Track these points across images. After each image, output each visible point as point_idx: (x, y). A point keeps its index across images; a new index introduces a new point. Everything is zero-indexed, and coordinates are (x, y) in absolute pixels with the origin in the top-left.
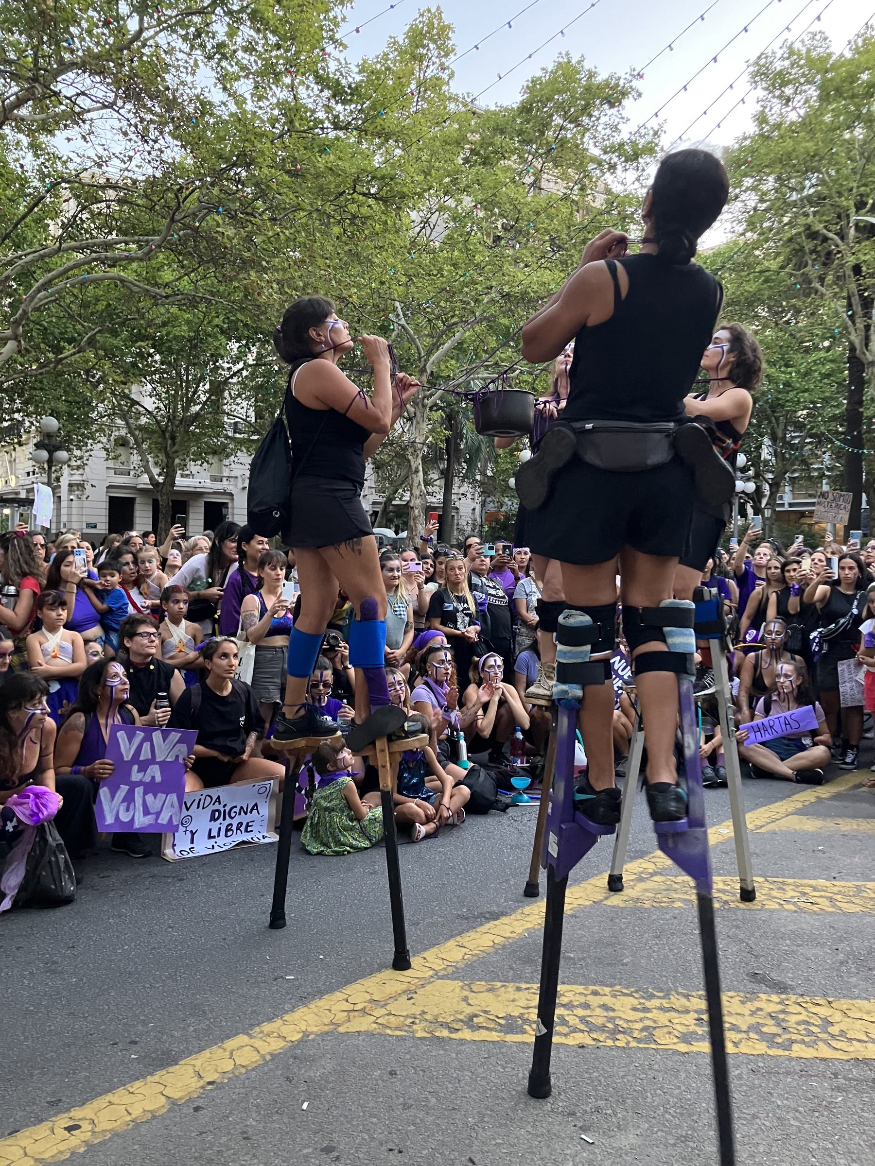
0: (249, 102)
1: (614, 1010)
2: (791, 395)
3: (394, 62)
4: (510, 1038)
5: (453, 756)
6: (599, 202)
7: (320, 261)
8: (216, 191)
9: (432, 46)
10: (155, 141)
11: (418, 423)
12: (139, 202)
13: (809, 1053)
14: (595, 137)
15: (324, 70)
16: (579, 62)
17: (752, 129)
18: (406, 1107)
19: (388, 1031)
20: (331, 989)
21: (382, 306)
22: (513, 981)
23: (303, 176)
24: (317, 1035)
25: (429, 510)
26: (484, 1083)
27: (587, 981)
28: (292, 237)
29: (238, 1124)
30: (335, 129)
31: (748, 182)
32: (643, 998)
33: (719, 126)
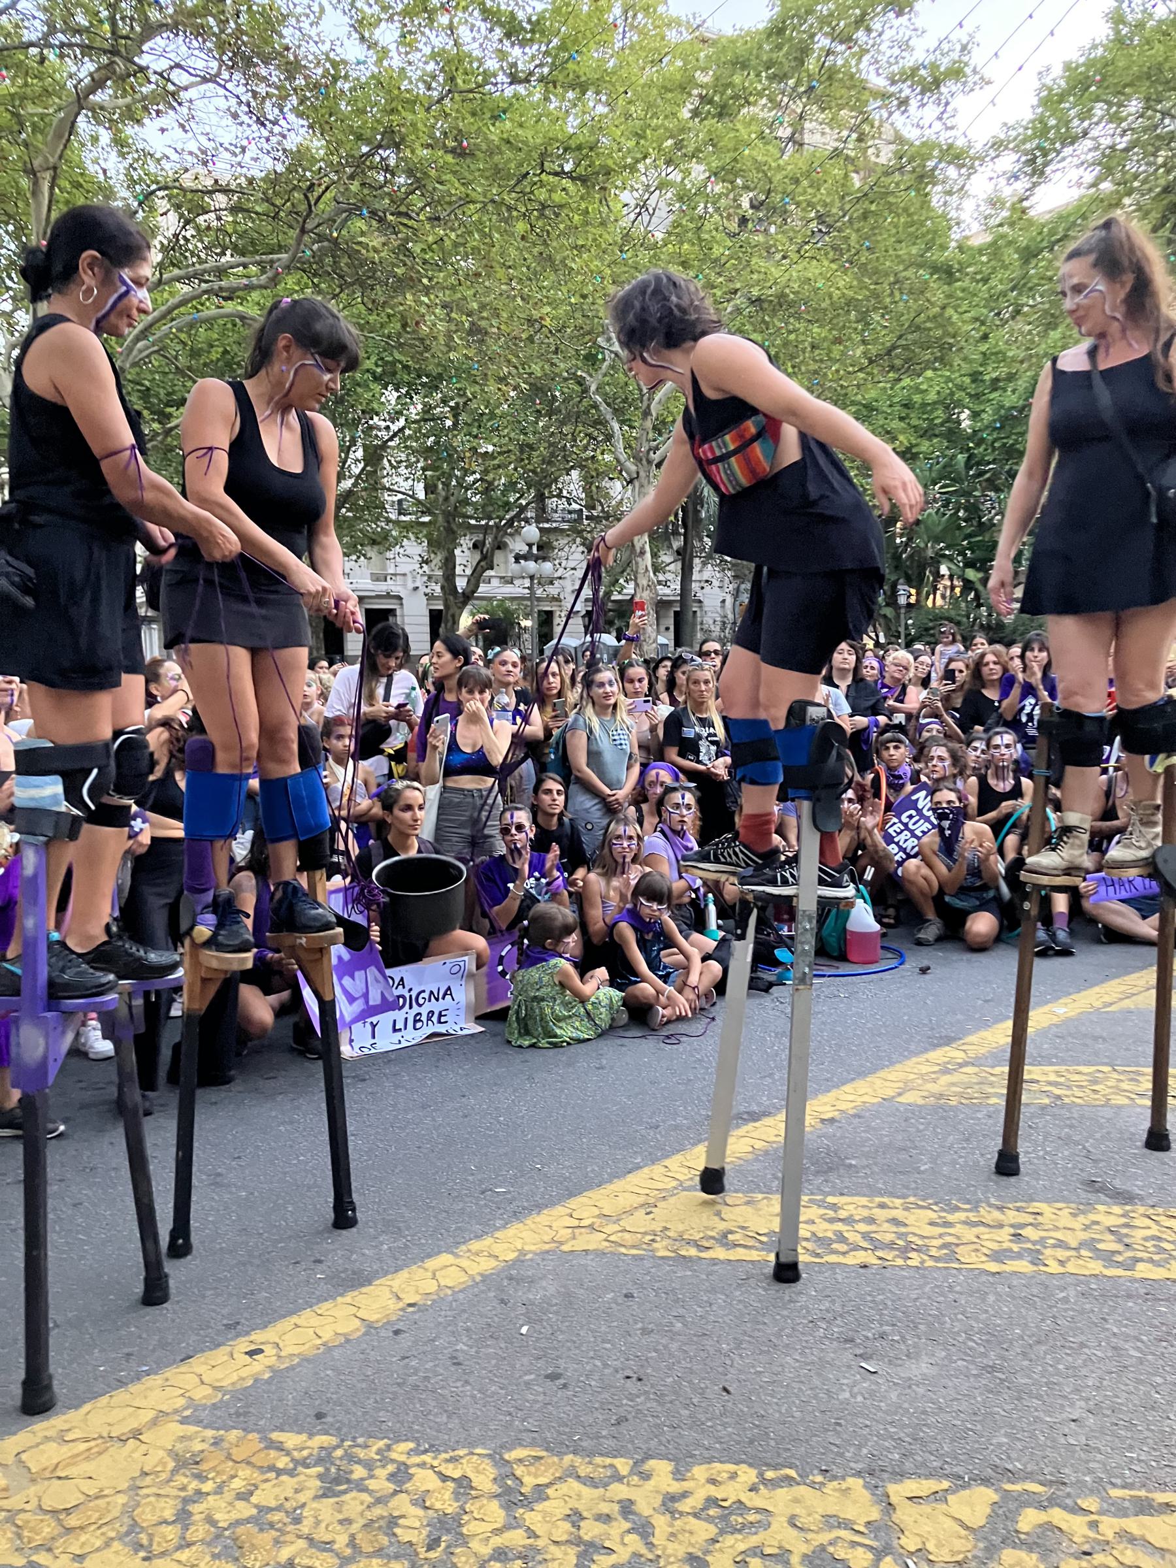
0: (393, 54)
5: (700, 925)
7: (501, 273)
8: (355, 187)
11: (642, 486)
12: (258, 209)
13: (1158, 1273)
14: (877, 62)
18: (645, 1332)
19: (623, 1250)
20: (551, 1203)
21: (587, 328)
23: (472, 155)
25: (662, 605)
26: (741, 1306)
27: (872, 1192)
28: (460, 240)
31: (1099, 109)
32: (943, 1210)
33: (1052, 34)
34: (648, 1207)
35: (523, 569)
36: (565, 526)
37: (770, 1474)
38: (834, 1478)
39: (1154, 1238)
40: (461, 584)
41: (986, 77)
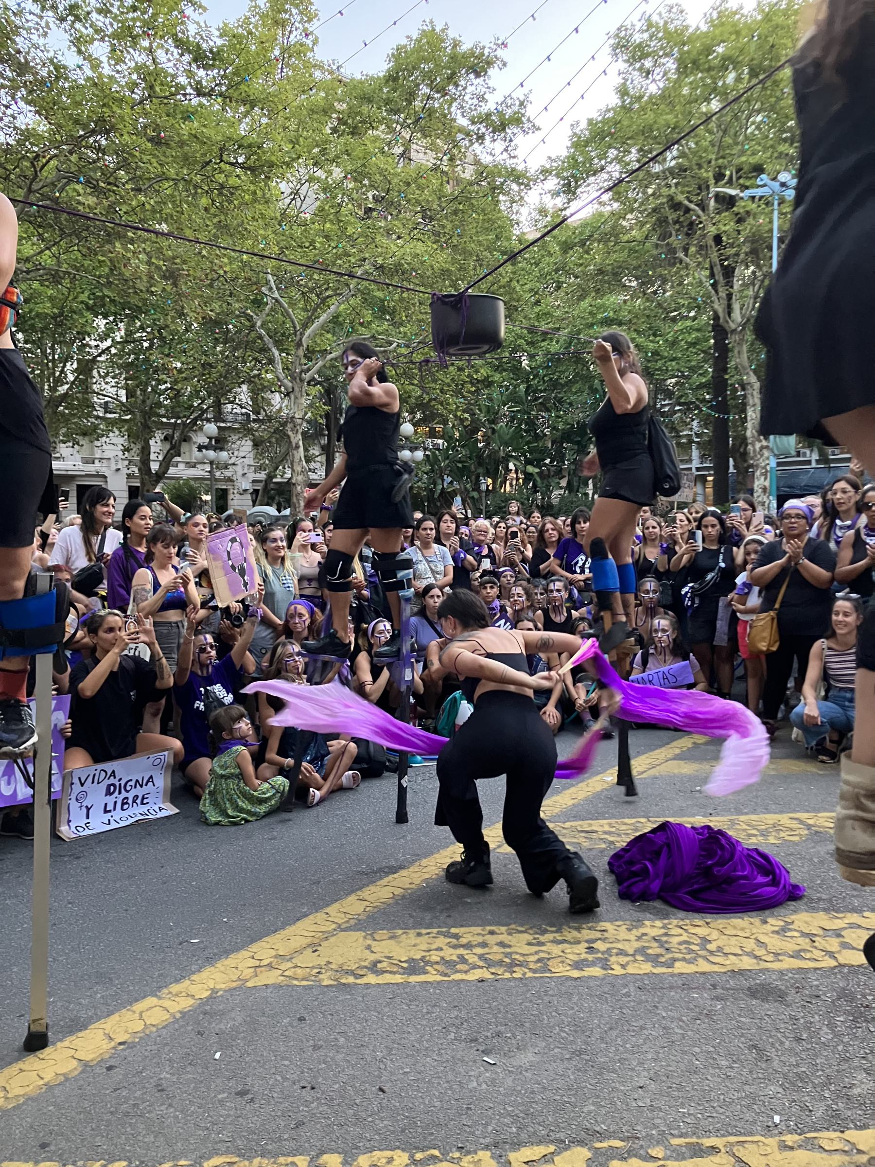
0: (105, 65)
1: (510, 946)
2: (659, 364)
3: (256, 27)
4: (413, 979)
6: (468, 174)
8: (74, 158)
9: (294, 11)
10: (7, 107)
11: (296, 398)
14: (462, 107)
15: (183, 33)
16: (443, 31)
17: (614, 100)
18: (316, 1048)
19: (295, 982)
22: (414, 928)
23: (167, 145)
24: (225, 991)
29: (152, 1078)
30: (198, 95)
31: (612, 153)
33: (582, 97)
34: (314, 947)
35: (205, 457)
36: (237, 426)
37: (419, 1156)
38: (468, 1153)
39: (685, 942)
40: (154, 467)
41: (537, 124)
